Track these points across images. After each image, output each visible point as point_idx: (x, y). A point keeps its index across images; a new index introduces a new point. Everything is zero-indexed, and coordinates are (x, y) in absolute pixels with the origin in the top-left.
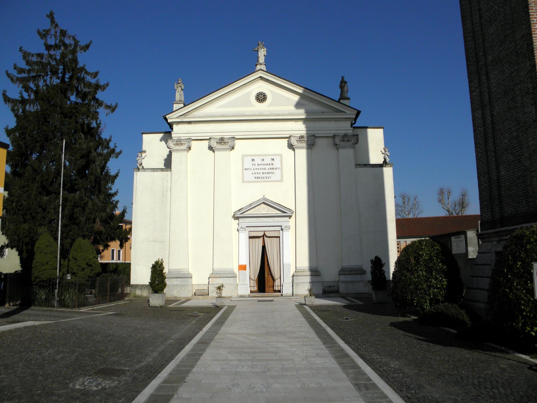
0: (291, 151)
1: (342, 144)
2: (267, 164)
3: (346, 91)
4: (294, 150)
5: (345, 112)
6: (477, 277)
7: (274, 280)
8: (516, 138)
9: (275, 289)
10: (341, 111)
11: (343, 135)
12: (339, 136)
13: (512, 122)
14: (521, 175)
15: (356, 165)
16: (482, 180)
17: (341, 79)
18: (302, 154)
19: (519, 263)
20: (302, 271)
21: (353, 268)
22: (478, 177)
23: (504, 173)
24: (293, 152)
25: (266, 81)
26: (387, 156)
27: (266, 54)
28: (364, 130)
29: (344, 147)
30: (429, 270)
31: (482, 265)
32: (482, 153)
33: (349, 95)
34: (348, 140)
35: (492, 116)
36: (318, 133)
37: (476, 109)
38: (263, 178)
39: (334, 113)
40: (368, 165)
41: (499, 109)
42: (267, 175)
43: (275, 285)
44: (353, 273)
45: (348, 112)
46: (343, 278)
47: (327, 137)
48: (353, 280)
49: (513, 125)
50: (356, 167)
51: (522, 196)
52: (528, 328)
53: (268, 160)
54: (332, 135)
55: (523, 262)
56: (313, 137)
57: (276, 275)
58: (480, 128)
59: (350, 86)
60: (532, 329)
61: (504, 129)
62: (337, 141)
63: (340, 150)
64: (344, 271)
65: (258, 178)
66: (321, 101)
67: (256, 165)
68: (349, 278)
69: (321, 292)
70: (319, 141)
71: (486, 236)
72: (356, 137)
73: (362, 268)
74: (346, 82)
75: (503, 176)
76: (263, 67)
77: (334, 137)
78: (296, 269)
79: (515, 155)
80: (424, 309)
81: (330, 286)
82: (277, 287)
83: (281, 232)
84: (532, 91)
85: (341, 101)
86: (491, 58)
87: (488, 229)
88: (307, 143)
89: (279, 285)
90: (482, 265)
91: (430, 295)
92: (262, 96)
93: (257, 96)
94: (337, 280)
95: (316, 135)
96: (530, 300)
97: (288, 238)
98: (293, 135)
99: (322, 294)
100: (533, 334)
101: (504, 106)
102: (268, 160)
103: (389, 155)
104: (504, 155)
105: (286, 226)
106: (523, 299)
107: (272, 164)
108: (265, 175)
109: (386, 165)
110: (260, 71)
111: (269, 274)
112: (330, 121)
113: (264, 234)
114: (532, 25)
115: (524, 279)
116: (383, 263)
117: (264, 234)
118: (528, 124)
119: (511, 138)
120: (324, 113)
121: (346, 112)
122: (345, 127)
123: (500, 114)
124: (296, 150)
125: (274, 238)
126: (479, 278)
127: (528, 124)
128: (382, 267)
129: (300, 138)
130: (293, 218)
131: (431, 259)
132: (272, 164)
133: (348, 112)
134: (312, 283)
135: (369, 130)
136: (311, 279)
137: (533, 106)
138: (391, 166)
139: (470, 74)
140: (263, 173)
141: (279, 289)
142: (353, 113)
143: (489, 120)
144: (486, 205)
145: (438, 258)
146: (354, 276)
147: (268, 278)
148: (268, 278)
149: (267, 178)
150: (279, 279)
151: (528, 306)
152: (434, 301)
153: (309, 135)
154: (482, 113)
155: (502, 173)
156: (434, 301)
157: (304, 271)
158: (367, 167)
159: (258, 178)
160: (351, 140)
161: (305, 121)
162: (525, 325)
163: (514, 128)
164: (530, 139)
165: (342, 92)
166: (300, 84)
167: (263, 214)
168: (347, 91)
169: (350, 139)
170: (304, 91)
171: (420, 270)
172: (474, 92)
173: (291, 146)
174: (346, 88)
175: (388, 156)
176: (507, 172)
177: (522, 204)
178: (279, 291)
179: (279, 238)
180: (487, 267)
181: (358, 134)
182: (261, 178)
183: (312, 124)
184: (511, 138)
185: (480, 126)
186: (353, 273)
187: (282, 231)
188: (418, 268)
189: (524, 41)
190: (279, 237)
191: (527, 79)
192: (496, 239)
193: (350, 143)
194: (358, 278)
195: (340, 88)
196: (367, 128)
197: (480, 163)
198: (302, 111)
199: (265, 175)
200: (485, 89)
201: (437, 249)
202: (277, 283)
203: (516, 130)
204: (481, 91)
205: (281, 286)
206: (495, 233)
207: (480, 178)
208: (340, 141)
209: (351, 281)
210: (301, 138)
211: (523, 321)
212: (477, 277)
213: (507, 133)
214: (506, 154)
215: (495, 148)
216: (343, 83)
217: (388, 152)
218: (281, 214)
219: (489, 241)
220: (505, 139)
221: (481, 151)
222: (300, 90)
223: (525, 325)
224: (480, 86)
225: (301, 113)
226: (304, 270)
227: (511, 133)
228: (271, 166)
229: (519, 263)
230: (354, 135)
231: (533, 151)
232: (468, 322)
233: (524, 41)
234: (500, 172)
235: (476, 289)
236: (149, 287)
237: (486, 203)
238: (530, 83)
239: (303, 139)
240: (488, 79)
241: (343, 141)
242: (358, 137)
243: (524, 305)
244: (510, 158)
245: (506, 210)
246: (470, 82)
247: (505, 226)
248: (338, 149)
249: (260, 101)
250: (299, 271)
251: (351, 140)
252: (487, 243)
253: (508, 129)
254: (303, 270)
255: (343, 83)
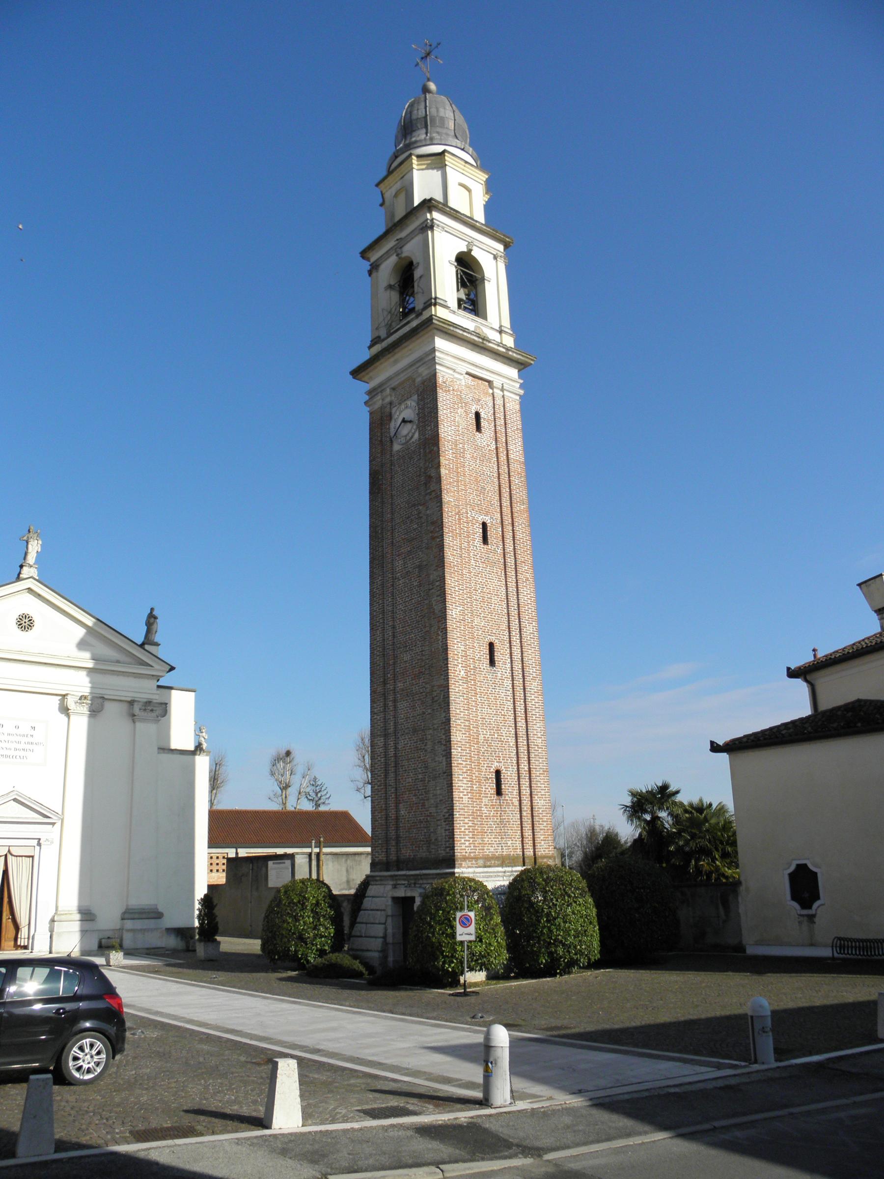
0: (63, 718)
1: (143, 714)
2: (24, 736)
3: (154, 632)
4: (68, 716)
5: (152, 666)
6: (366, 923)
7: (17, 928)
8: (421, 781)
9: (19, 944)
10: (147, 663)
11: (145, 700)
12: (139, 701)
13: (419, 763)
14: (423, 819)
15: (159, 748)
16: (378, 816)
17: (149, 612)
18: (81, 722)
19: (441, 912)
20: (66, 914)
21: (144, 909)
22: (371, 811)
23: (405, 813)
24: (66, 719)
25: (37, 596)
26: (203, 739)
27: (39, 550)
28: (167, 690)
29: (144, 720)
30: (316, 915)
31: (372, 910)
32: (380, 786)
33: (157, 638)
34: (152, 710)
35: (396, 748)
36: (108, 694)
37: (378, 735)
38: (14, 757)
39: (136, 666)
40: (166, 749)
41: (405, 744)
42: (22, 753)
43: (19, 936)
44: (144, 916)
45: (156, 666)
46: (129, 924)
47: (121, 701)
48: (145, 927)
49: (419, 766)
50: (158, 753)
51: (423, 841)
52: (447, 966)
53: (25, 729)
54: (129, 699)
55: (444, 911)
56: (101, 700)
57: (22, 918)
58: (381, 758)
59: (161, 626)
60: (450, 965)
61: (408, 767)
62: (136, 709)
63: (138, 724)
64: (129, 914)
65: (7, 756)
66: (102, 632)
67: (6, 734)
68: (138, 924)
69: (95, 946)
70: (108, 706)
71: (378, 878)
72: (164, 706)
73: (158, 909)
74: (156, 618)
75: (403, 816)
76: (33, 572)
77: (131, 703)
78: (57, 909)
79: (419, 798)
80: (308, 961)
81: (109, 938)
82: (23, 940)
83: (37, 848)
84: (444, 743)
85: (147, 647)
86: (401, 686)
87: (381, 871)
88: (90, 707)
89: (27, 937)
90: (372, 910)
91: (317, 945)
92: (23, 622)
93: (20, 619)
94: (118, 927)
95: (106, 697)
96: (449, 942)
97: (47, 857)
98: (72, 693)
99: (98, 950)
100: (450, 969)
101: (411, 743)
102: (25, 729)
103: (206, 737)
104: (406, 794)
105: (47, 840)
106: (444, 942)
107: (32, 736)
108: (18, 753)
109: (200, 753)
110: (31, 579)
111: (9, 918)
112: (135, 678)
113: (9, 851)
114: (450, 679)
115: (444, 926)
116: (215, 904)
117: (9, 851)
118: (437, 773)
119: (416, 779)
120: (120, 663)
121: (153, 665)
122: (145, 689)
123: (405, 750)
124: (72, 717)
125: (24, 858)
126: (368, 925)
127: (437, 773)
128: (213, 909)
129: (80, 699)
130: (58, 826)
131: (317, 904)
132: (32, 736)
133: (156, 666)
134: (84, 932)
135: (173, 692)
136: (81, 926)
137: (444, 758)
138: (207, 755)
139: (373, 692)
140: (16, 749)
141: (26, 944)
142: (163, 669)
143: (391, 752)
144: (379, 844)
145: (325, 903)
146: (146, 921)
147: (6, 926)
148: (6, 926)
149: (22, 757)
150: (27, 926)
151: (448, 947)
152: (322, 953)
153: (94, 695)
154: (385, 742)
155: (402, 812)
156: (322, 953)
157: (70, 914)
158: (173, 754)
159: (7, 756)
160: (156, 710)
161: (91, 671)
162: (444, 963)
163: (420, 770)
164: (438, 788)
165: (149, 632)
166: (88, 610)
167: (12, 818)
168: (156, 632)
169: (155, 709)
170: (95, 624)
171: (307, 916)
172: (378, 716)
173: (65, 710)
174: (154, 627)
175: (205, 739)
176: (408, 813)
177: (423, 849)
178: (25, 947)
179: (31, 859)
180: (379, 913)
181: (166, 702)
182: (11, 757)
183: (100, 678)
184: (416, 779)
185: (380, 755)
186: (144, 916)
187: (39, 847)
188: (304, 913)
189: (441, 691)
190: (33, 857)
191: (441, 729)
192: (391, 883)
193: (154, 714)
194: (150, 924)
195: (146, 625)
196: (171, 688)
197: (376, 796)
198: (87, 655)
199: (18, 753)
200: (391, 717)
201: (324, 891)
202: (24, 933)
203: (423, 773)
204: (385, 717)
205: (28, 938)
206: (391, 876)
207: (375, 813)
208: (140, 709)
209: (141, 930)
210: (83, 698)
211: (443, 960)
212: (366, 923)
213: (412, 772)
214: (409, 794)
215: (396, 785)
216: (151, 619)
217: (206, 733)
218: (39, 818)
219: (381, 885)
220: (408, 778)
221: (378, 784)
222: (90, 621)
223: (444, 963)
224: (385, 711)
225: (85, 659)
226: (70, 912)
227: (416, 774)
228: (30, 739)
229: (441, 912)
230: (161, 704)
231: (440, 801)
232: (364, 972)
233: (441, 691)
234: (400, 811)
235: (366, 937)
236: (221, 928)
237: (380, 842)
238: (444, 734)
239: (85, 701)
240: (395, 707)
241: (145, 710)
242: (167, 707)
243: (445, 947)
244: (412, 799)
245: (403, 852)
246: (373, 701)
247: (402, 870)
248: (134, 722)
249: (23, 628)
250: (62, 913)
251: (156, 710)
252: (378, 886)
253: (414, 769)
254: (69, 911)
255: (151, 619)
